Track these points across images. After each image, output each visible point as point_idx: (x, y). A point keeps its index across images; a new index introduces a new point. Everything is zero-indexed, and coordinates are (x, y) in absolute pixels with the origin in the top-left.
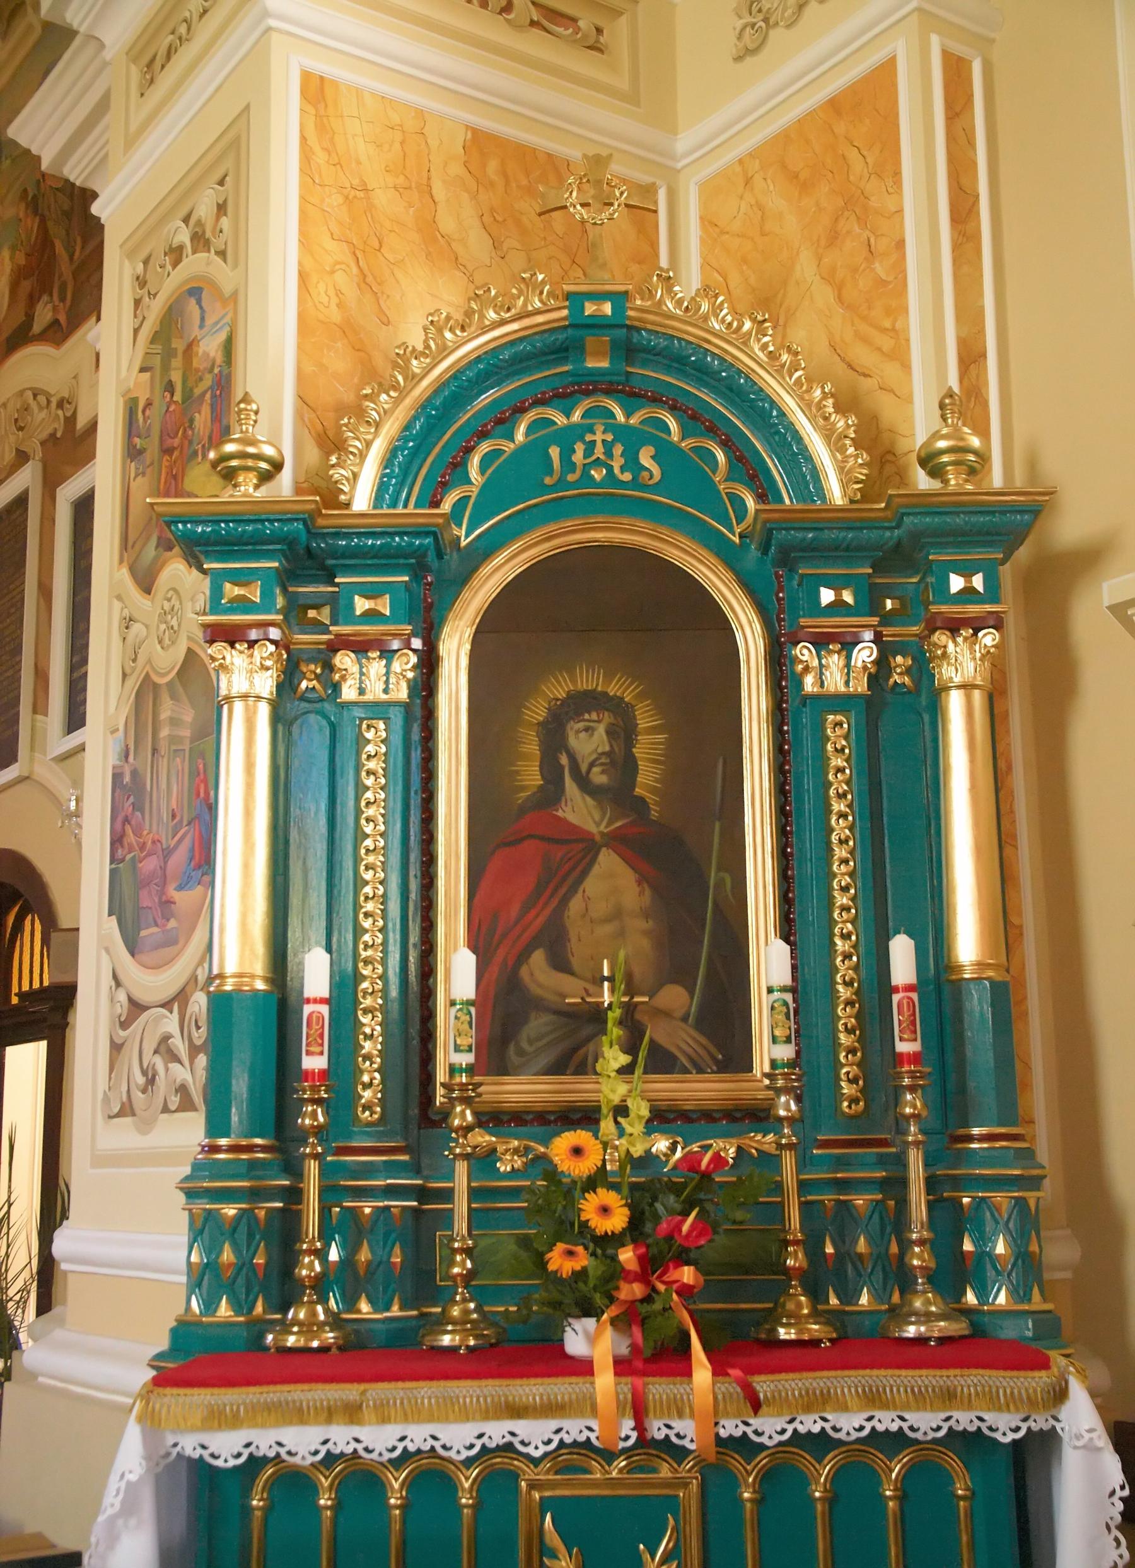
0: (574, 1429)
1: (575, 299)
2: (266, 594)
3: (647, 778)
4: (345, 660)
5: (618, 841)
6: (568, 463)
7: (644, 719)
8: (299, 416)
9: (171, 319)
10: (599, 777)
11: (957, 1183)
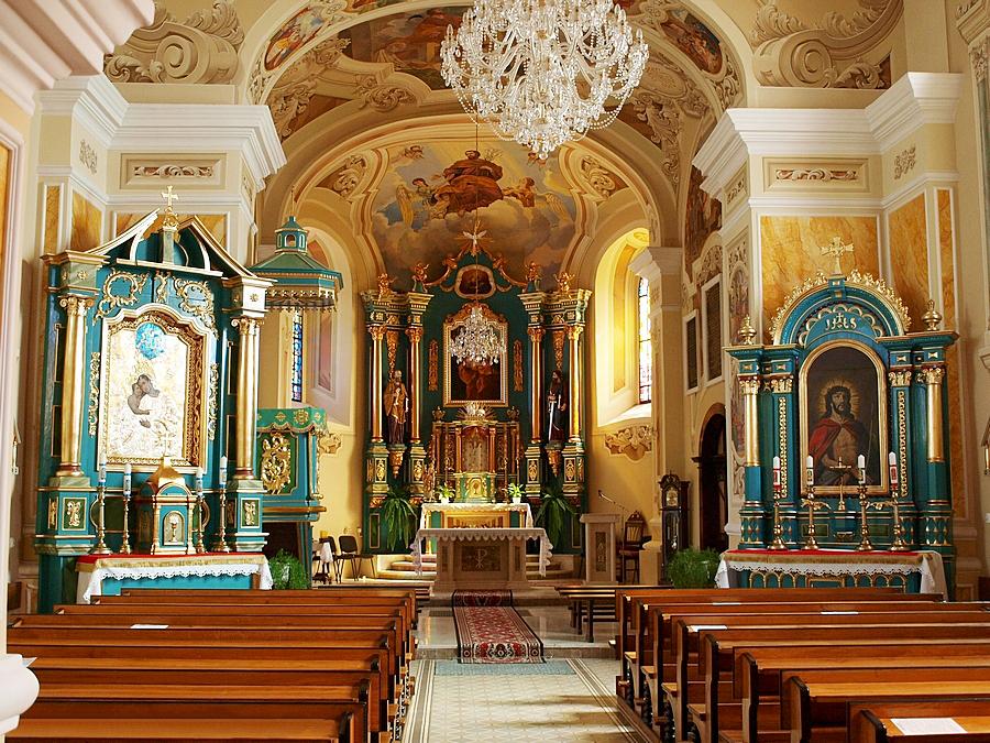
3: (853, 409)
4: (774, 382)
5: (845, 425)
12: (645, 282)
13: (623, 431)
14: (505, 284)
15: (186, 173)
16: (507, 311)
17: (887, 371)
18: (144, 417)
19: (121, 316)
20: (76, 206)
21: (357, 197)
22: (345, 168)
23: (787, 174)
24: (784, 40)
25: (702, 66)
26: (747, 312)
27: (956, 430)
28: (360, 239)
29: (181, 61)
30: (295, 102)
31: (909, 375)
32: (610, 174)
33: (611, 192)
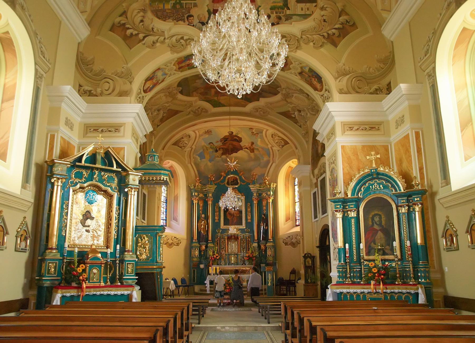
0: (370, 291)
1: (371, 170)
2: (340, 207)
3: (383, 223)
4: (349, 212)
5: (380, 230)
6: (372, 188)
7: (383, 216)
8: (344, 184)
9: (332, 170)
10: (378, 223)
11: (417, 268)
12: (297, 180)
13: (289, 237)
14: (243, 181)
15: (110, 131)
16: (243, 190)
17: (397, 207)
18: (87, 228)
19: (78, 186)
20: (62, 142)
21: (188, 149)
22: (182, 138)
23: (351, 129)
24: (348, 76)
25: (316, 89)
26: (337, 185)
27: (429, 231)
28: (189, 165)
29: (109, 88)
30: (162, 112)
31: (407, 208)
32: (283, 139)
33: (283, 146)
